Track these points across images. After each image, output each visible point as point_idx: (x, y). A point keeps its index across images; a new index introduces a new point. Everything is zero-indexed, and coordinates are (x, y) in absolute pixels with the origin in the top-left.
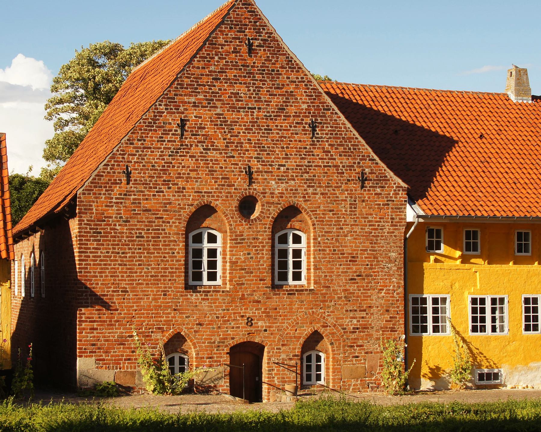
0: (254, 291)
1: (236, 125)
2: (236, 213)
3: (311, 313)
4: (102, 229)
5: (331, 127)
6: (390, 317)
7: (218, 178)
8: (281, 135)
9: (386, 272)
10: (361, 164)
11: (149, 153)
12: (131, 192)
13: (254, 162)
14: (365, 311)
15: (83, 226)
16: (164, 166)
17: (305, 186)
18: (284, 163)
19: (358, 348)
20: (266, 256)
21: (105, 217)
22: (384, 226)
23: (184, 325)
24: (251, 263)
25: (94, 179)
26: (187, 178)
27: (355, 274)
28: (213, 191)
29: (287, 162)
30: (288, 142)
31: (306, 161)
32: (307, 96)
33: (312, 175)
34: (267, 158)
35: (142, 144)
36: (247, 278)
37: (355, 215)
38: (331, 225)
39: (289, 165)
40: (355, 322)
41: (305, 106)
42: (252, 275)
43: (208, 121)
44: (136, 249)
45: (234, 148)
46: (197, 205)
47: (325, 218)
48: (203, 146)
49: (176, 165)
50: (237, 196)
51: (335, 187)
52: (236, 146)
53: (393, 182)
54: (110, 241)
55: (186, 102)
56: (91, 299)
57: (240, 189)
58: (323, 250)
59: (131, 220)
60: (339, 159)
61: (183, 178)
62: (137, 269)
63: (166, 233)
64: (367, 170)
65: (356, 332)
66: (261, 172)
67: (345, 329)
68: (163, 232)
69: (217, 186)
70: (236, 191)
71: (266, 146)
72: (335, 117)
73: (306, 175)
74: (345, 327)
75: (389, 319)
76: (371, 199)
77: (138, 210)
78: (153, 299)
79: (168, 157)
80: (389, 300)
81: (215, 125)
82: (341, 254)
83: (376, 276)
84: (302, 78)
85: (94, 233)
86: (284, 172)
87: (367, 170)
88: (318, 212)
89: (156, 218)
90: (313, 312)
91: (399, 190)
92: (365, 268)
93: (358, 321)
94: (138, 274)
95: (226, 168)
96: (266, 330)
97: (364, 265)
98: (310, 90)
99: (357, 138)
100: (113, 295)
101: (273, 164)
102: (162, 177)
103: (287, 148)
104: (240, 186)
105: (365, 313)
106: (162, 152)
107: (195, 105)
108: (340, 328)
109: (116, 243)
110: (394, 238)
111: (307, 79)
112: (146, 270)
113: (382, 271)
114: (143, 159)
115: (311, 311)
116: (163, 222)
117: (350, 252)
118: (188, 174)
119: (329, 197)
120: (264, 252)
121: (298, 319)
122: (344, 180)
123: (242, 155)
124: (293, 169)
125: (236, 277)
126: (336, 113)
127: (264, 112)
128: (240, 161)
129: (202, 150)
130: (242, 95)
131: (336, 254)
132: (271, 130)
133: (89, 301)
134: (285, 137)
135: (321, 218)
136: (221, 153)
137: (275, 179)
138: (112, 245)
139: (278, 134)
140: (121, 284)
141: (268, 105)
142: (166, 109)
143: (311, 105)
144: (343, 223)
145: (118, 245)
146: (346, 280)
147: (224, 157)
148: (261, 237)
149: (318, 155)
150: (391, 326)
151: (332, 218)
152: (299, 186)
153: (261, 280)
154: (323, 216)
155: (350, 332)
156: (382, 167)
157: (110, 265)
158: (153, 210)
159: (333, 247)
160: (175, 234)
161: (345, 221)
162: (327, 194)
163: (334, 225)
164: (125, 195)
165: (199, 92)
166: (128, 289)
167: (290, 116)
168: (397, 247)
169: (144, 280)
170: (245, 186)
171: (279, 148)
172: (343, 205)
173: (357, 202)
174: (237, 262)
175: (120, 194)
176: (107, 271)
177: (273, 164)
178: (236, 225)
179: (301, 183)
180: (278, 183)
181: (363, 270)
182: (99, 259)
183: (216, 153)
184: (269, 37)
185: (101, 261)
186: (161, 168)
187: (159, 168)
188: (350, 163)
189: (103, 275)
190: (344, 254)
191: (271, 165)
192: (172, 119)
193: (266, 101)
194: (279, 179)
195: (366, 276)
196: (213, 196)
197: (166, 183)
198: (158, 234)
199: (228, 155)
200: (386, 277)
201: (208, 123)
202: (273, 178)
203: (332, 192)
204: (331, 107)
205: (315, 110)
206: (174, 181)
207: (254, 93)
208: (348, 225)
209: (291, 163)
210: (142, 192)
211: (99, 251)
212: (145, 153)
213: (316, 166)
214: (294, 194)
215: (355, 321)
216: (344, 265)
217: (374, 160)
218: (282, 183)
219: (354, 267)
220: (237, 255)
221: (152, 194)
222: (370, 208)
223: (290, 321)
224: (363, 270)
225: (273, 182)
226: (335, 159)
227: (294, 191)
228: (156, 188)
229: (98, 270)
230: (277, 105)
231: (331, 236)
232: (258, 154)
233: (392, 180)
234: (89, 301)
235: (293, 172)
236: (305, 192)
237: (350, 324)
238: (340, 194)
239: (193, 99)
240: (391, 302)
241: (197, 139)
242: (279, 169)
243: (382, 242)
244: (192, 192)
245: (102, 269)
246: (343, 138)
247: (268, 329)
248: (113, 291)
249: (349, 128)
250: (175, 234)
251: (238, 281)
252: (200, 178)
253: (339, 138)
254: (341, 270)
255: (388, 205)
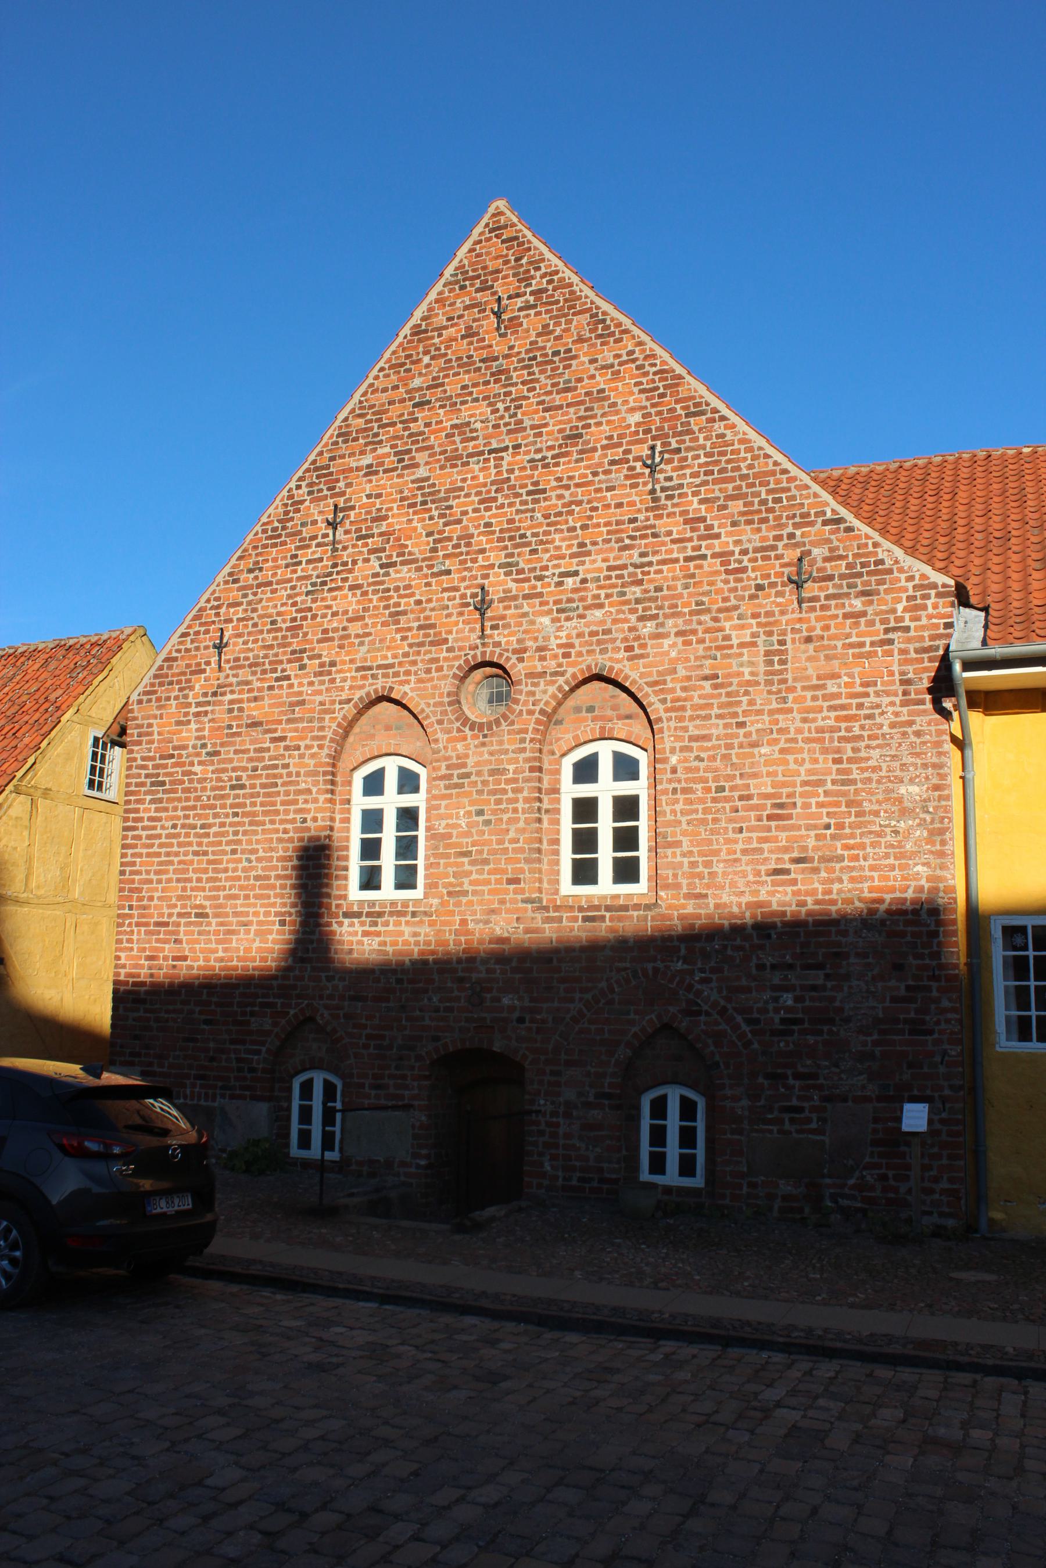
0: (493, 911)
1: (459, 497)
2: (449, 709)
3: (650, 972)
4: (166, 775)
5: (706, 455)
6: (908, 988)
7: (410, 629)
8: (568, 499)
9: (892, 846)
10: (798, 539)
11: (269, 595)
12: (225, 686)
13: (498, 575)
14: (820, 966)
15: (135, 771)
16: (294, 620)
17: (633, 618)
18: (575, 568)
19: (797, 1083)
20: (522, 817)
21: (175, 748)
22: (878, 706)
23: (321, 997)
24: (486, 837)
25: (161, 668)
26: (342, 638)
27: (786, 857)
28: (396, 661)
29: (583, 563)
30: (589, 513)
31: (635, 553)
32: (641, 391)
33: (652, 587)
34: (529, 561)
35: (256, 578)
36: (474, 876)
37: (785, 681)
38: (708, 717)
39: (588, 571)
40: (790, 1002)
41: (637, 417)
42: (486, 868)
43: (394, 501)
44: (227, 815)
45: (450, 550)
46: (361, 699)
47: (691, 698)
48: (380, 559)
49: (319, 613)
50: (452, 667)
51: (720, 610)
52: (457, 546)
53: (903, 576)
54: (179, 800)
55: (351, 470)
56: (139, 932)
57: (460, 649)
58: (684, 791)
59: (222, 750)
60: (729, 534)
61: (332, 639)
62: (228, 862)
63: (289, 775)
64: (816, 551)
65: (791, 1033)
66: (515, 598)
67: (757, 1021)
68: (284, 771)
69: (407, 649)
70: (451, 655)
71: (529, 534)
72: (719, 427)
73: (634, 589)
74: (755, 1015)
75: (903, 992)
76: (833, 631)
77: (238, 726)
78: (257, 933)
79: (304, 597)
80: (903, 934)
81: (410, 506)
82: (741, 798)
83: (855, 858)
84: (630, 353)
85: (153, 784)
86: (575, 590)
87: (818, 552)
88: (670, 685)
89: (274, 740)
90: (656, 970)
91: (926, 597)
92: (818, 837)
93: (797, 999)
94: (230, 874)
95: (429, 601)
96: (521, 1020)
97: (815, 827)
98: (651, 377)
99: (785, 471)
100: (178, 925)
101: (547, 573)
102: (290, 644)
103: (584, 527)
104: (462, 639)
105: (821, 973)
106: (293, 588)
107: (370, 471)
108: (739, 1019)
109: (191, 803)
110: (913, 738)
111: (612, 320)
112: (245, 864)
113: (873, 845)
114: (254, 610)
115: (650, 966)
116: (287, 748)
117: (770, 790)
118: (344, 629)
119: (701, 641)
120: (520, 805)
121: (612, 991)
122: (744, 589)
123: (469, 564)
124: (598, 579)
125: (447, 876)
126: (723, 418)
127: (528, 452)
128: (463, 579)
129: (378, 569)
130: (478, 425)
131: (727, 799)
132: (544, 491)
133: (135, 937)
134: (579, 503)
135: (678, 700)
136: (419, 569)
137: (549, 612)
138: (184, 809)
139: (560, 497)
140: (196, 897)
141: (540, 434)
142: (310, 493)
143: (653, 411)
144: (744, 707)
145: (194, 808)
146: (758, 873)
147: (426, 576)
148: (511, 768)
149: (669, 533)
150: (912, 1015)
151: (712, 696)
152: (615, 621)
153: (510, 881)
154: (684, 695)
155: (773, 1033)
156: (867, 537)
157: (177, 854)
158: (268, 723)
159: (716, 779)
160: (308, 774)
161: (751, 703)
162: (694, 632)
163: (718, 717)
164: (215, 694)
165: (381, 442)
166: (208, 910)
167: (594, 450)
168: (925, 766)
169: (241, 888)
170: (474, 638)
171: (562, 531)
172: (745, 658)
173: (789, 645)
174: (449, 836)
175: (205, 695)
176: (171, 868)
177: (547, 573)
178: (449, 740)
179: (619, 612)
180: (558, 620)
181: (811, 842)
182: (157, 842)
183: (410, 570)
184: (549, 282)
185: (161, 846)
186: (288, 624)
187: (284, 626)
188: (763, 539)
189: (164, 877)
190: (749, 797)
191: (539, 578)
192: (320, 512)
193: (533, 427)
194: (559, 611)
195: (823, 859)
196: (396, 674)
197: (297, 656)
198: (275, 776)
199: (435, 570)
200: (891, 861)
201: (395, 506)
202: (546, 608)
203: (711, 624)
204: (707, 404)
205: (664, 420)
206: (313, 649)
207: (507, 415)
208: (760, 712)
209: (594, 565)
210: (247, 683)
211: (159, 824)
212: (259, 596)
213: (663, 562)
214: (599, 642)
215: (788, 999)
216: (750, 829)
217: (840, 521)
218: (568, 619)
219: (783, 835)
220: (450, 816)
221: (266, 685)
222: (828, 658)
223: (588, 996)
224: (811, 842)
225: (546, 620)
226: (717, 536)
227: (601, 637)
228: (275, 671)
229: (155, 867)
230: (560, 431)
231: (708, 749)
232: (507, 556)
233: (901, 570)
234: (135, 937)
235: (600, 587)
236: (632, 635)
237: (771, 1006)
238: (734, 628)
239: (367, 460)
240: (909, 939)
241: (367, 544)
242: (560, 584)
243: (875, 753)
244: (350, 670)
245: (160, 864)
246: (743, 477)
247: (528, 1017)
248: (180, 915)
249: (760, 448)
250: (308, 774)
251: (451, 884)
252: (369, 634)
253: (732, 479)
254: (740, 846)
255: (891, 642)
